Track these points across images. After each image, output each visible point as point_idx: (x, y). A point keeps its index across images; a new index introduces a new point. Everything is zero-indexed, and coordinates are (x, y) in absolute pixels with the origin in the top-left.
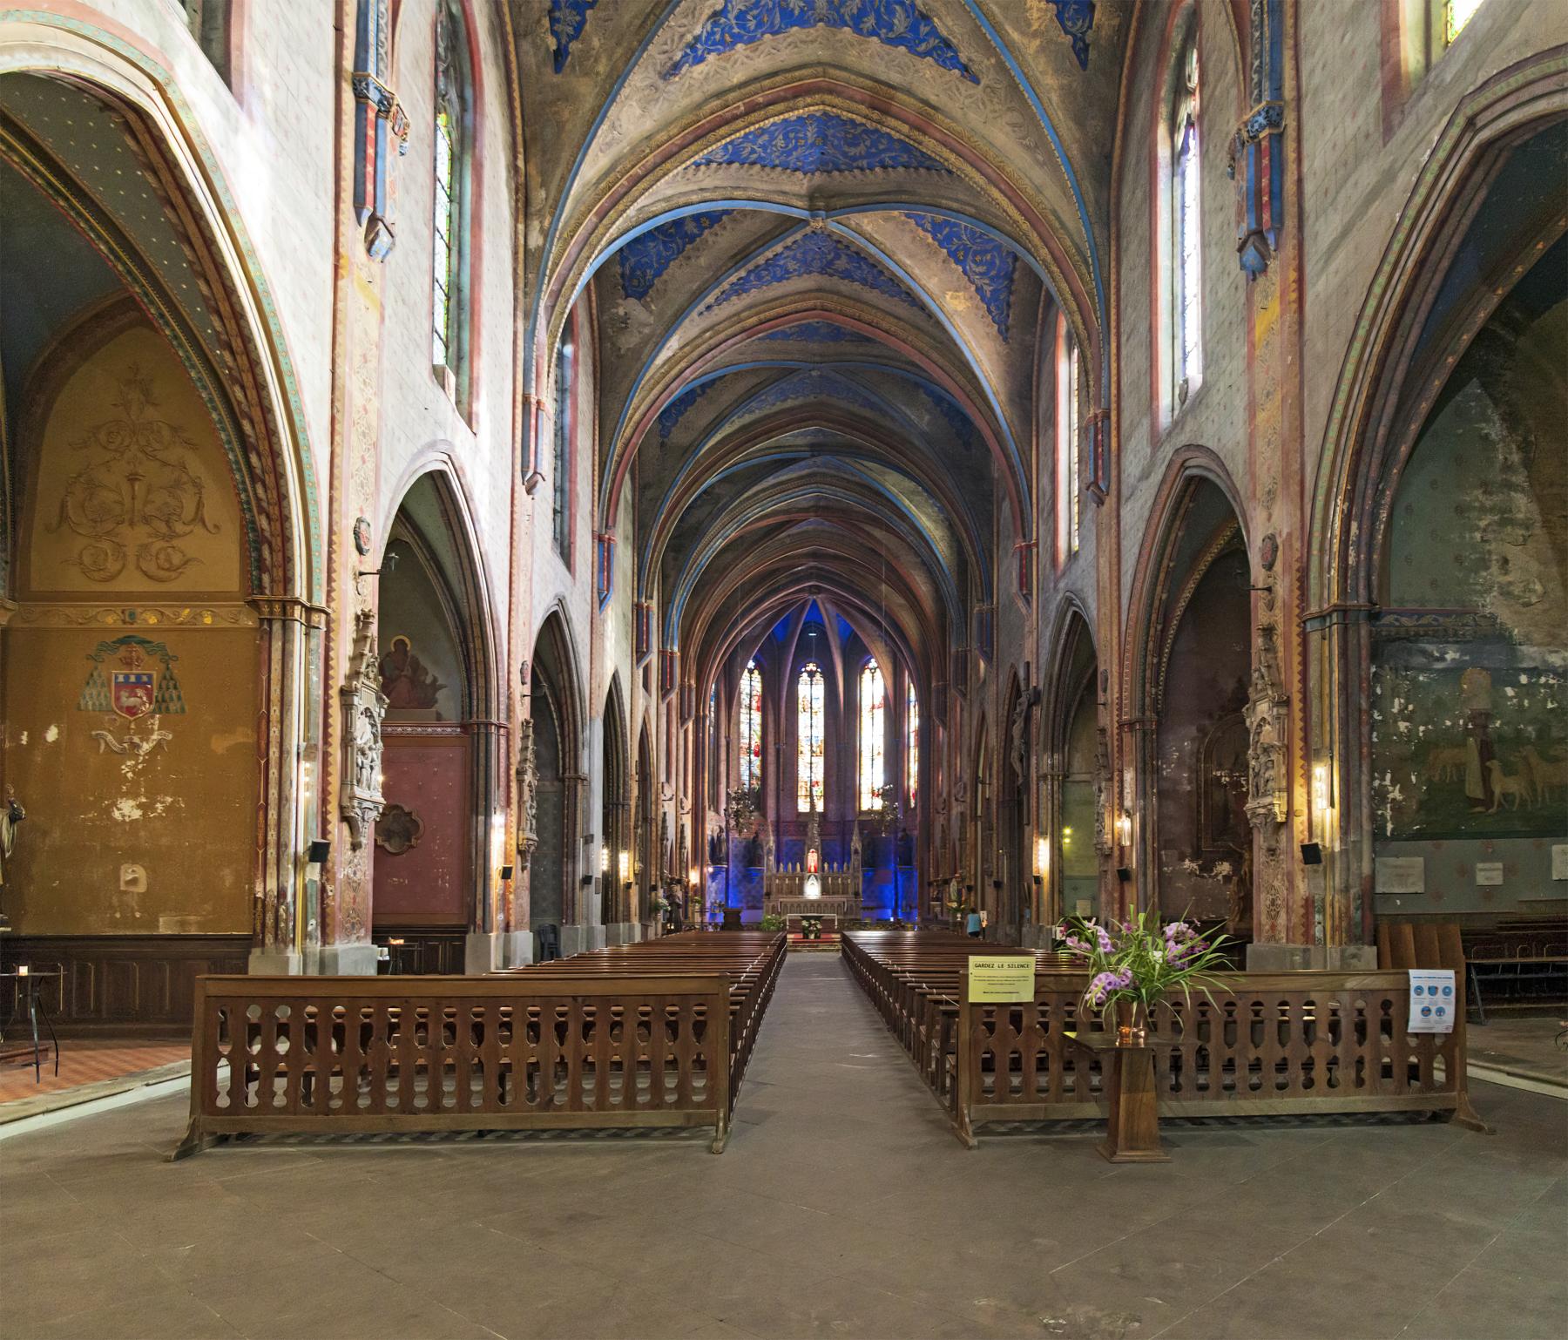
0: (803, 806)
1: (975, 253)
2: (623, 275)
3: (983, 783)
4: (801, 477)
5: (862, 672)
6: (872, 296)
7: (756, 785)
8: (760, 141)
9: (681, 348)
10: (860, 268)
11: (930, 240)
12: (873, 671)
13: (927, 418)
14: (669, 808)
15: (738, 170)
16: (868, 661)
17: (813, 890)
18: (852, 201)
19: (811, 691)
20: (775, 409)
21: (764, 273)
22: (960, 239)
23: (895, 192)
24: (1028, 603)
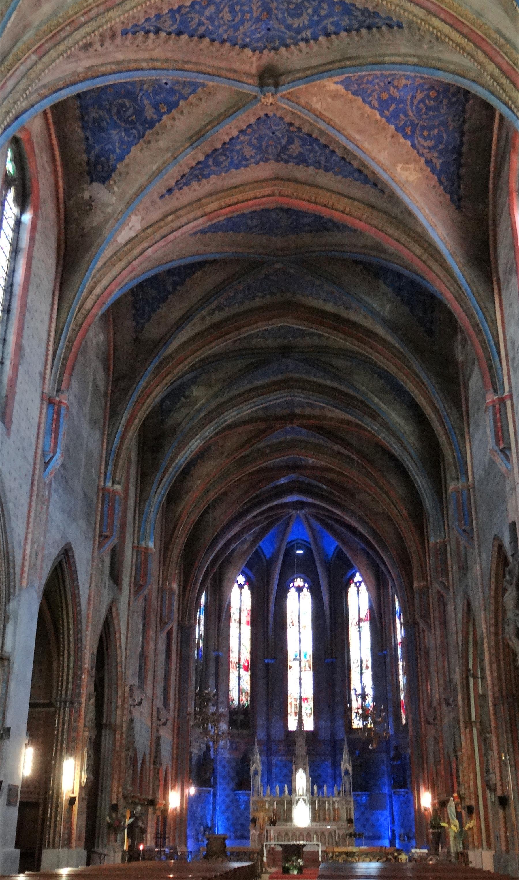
0: (292, 725)
1: (423, 128)
2: (88, 163)
3: (475, 677)
4: (274, 383)
5: (347, 586)
6: (325, 179)
7: (245, 701)
8: (207, 13)
9: (144, 230)
10: (312, 151)
11: (378, 116)
12: (358, 585)
13: (388, 307)
14: (142, 718)
15: (187, 43)
16: (354, 575)
17: (302, 816)
18: (300, 75)
19: (299, 606)
20: (243, 308)
21: (222, 158)
22: (406, 115)
23: (340, 61)
24: (508, 458)
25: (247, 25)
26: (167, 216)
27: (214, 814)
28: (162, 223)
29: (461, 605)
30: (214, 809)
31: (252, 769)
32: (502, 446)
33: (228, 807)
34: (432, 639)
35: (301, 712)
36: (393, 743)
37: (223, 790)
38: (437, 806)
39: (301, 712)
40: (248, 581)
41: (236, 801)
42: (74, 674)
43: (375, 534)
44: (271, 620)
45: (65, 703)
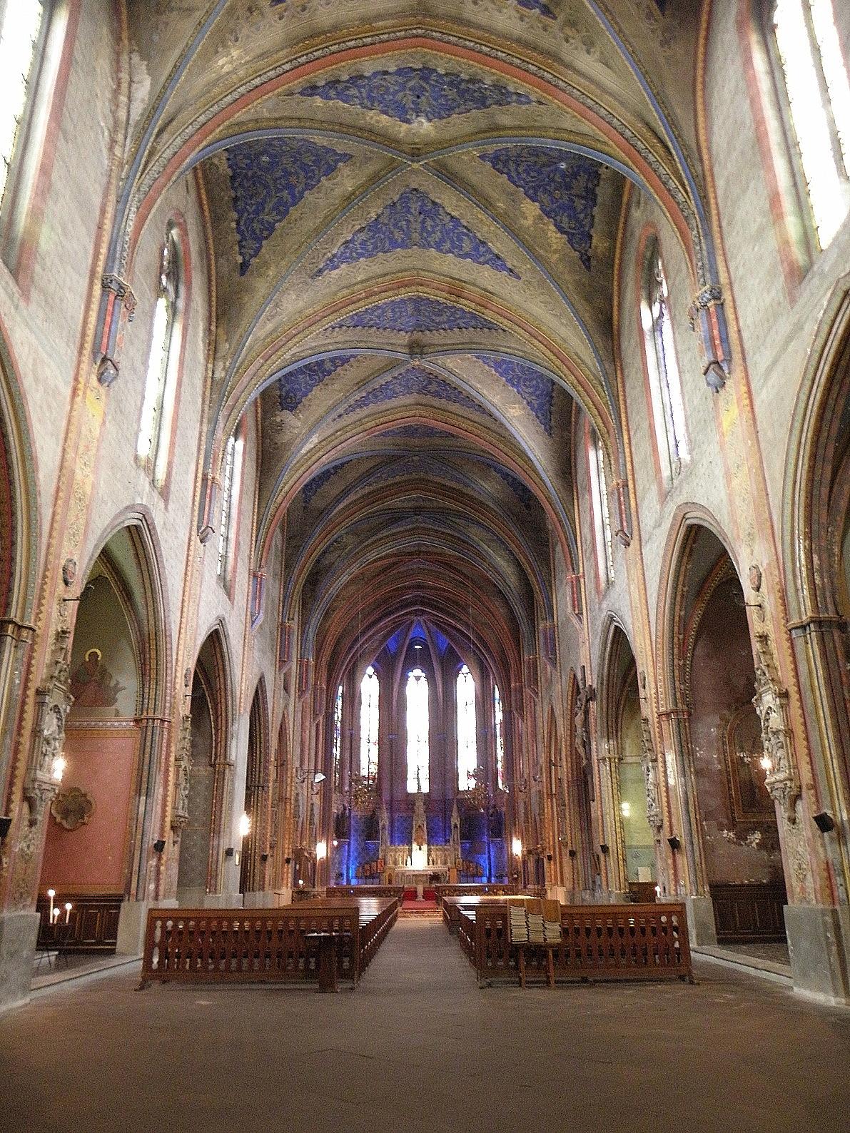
11: (494, 372)
16: (462, 667)
19: (417, 690)
25: (403, 319)
26: (337, 432)
27: (348, 860)
28: (333, 437)
29: (546, 708)
30: (349, 855)
31: (381, 824)
32: (577, 612)
33: (360, 853)
34: (522, 726)
35: (418, 778)
36: (492, 803)
37: (354, 842)
38: (525, 853)
39: (418, 778)
40: (377, 671)
41: (365, 849)
42: (265, 765)
43: (481, 639)
44: (394, 703)
45: (258, 787)
